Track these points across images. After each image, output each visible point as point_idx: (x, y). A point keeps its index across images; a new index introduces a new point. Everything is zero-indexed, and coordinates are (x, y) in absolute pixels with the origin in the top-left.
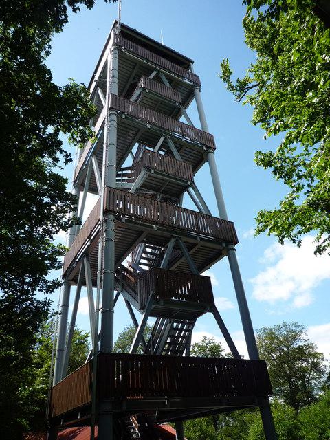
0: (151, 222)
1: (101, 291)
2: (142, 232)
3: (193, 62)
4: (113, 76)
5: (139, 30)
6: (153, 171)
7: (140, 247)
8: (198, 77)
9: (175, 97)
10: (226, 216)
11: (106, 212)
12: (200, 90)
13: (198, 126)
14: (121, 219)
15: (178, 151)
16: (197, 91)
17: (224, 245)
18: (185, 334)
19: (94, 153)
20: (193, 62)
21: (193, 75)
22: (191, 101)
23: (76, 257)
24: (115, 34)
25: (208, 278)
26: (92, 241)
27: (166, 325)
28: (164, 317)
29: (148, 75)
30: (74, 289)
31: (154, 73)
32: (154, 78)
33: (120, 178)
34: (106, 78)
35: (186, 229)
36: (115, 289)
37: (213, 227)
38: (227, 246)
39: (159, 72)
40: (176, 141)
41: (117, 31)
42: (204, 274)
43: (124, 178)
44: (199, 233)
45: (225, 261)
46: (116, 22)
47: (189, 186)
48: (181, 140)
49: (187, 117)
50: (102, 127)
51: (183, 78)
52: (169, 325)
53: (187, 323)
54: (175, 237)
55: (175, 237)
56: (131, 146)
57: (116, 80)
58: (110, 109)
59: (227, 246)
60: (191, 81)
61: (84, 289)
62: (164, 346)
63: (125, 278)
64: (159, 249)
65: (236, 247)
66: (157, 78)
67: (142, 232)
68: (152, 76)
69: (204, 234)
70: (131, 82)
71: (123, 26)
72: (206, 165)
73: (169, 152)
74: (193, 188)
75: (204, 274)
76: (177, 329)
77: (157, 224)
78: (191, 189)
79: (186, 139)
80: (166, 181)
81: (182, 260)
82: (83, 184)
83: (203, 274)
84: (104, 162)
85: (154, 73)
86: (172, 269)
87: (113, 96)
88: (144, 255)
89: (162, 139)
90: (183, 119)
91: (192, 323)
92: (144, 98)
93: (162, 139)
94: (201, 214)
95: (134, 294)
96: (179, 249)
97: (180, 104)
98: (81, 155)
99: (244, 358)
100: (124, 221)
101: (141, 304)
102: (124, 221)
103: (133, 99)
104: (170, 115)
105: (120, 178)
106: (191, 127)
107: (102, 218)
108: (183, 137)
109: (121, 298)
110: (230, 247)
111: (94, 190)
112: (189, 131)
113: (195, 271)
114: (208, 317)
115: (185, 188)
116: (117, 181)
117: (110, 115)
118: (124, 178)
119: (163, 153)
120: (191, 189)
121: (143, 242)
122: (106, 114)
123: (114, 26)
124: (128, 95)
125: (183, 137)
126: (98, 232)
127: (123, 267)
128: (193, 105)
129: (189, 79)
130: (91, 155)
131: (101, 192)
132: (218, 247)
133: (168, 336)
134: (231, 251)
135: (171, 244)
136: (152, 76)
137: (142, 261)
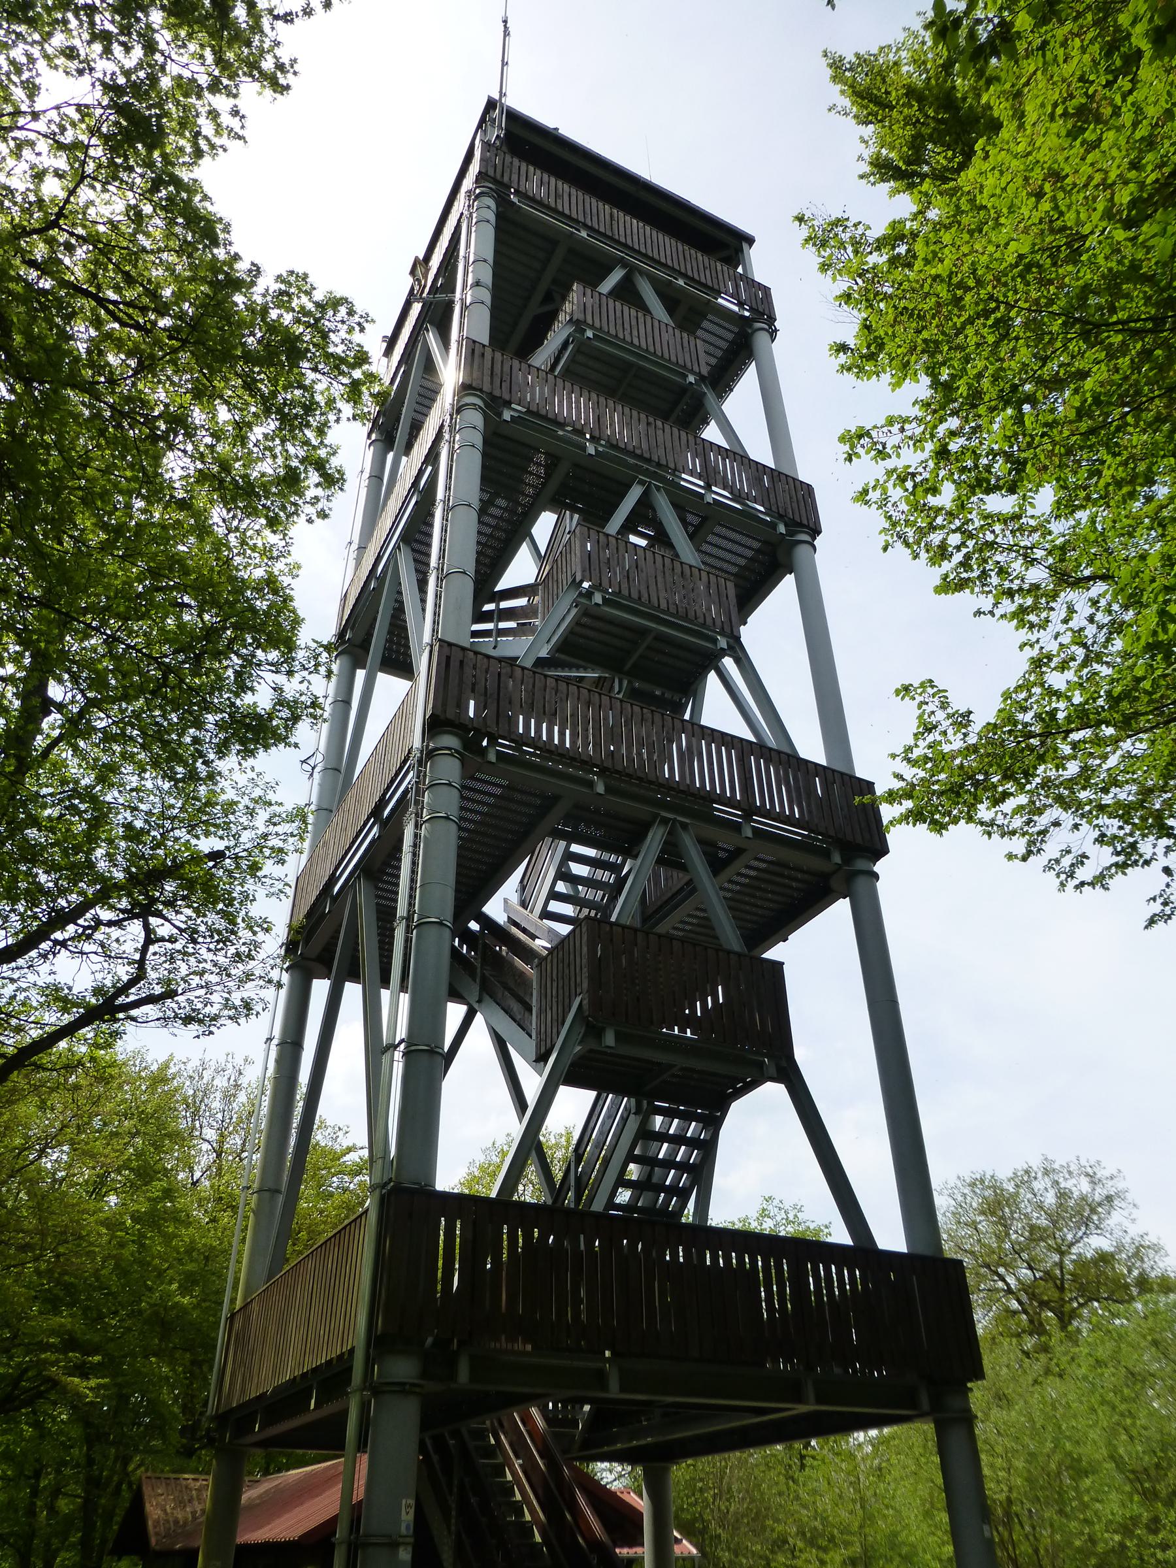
0: (586, 764)
1: (405, 999)
2: (555, 799)
3: (750, 241)
4: (477, 284)
5: (569, 131)
6: (589, 334)
7: (549, 856)
8: (766, 290)
9: (685, 358)
10: (852, 768)
11: (433, 726)
12: (773, 333)
13: (760, 451)
14: (483, 752)
15: (691, 537)
16: (761, 338)
17: (837, 858)
18: (677, 1179)
19: (405, 538)
20: (750, 241)
21: (752, 284)
22: (747, 365)
23: (333, 880)
24: (487, 145)
25: (780, 965)
26: (384, 824)
27: (624, 1120)
28: (620, 1091)
29: (593, 282)
30: (320, 989)
31: (615, 277)
32: (616, 293)
33: (489, 626)
34: (453, 291)
35: (710, 798)
36: (456, 995)
37: (802, 792)
38: (847, 860)
39: (631, 271)
40: (684, 502)
41: (493, 135)
42: (772, 954)
43: (502, 625)
44: (749, 810)
45: (840, 912)
46: (491, 105)
47: (723, 653)
48: (701, 496)
49: (727, 428)
50: (432, 457)
51: (718, 293)
52: (633, 1123)
53: (698, 1118)
54: (665, 821)
55: (665, 821)
56: (530, 517)
57: (486, 296)
58: (465, 388)
59: (847, 860)
60: (740, 304)
61: (353, 993)
62: (613, 1194)
63: (499, 963)
64: (614, 868)
65: (880, 867)
66: (626, 293)
67: (555, 799)
68: (607, 286)
69: (768, 814)
70: (535, 308)
71: (513, 117)
72: (787, 586)
73: (661, 539)
74: (738, 661)
75: (772, 954)
76: (663, 1137)
77: (604, 772)
78: (728, 663)
79: (720, 494)
80: (643, 632)
81: (687, 907)
82: (365, 645)
83: (765, 956)
84: (433, 562)
85: (615, 277)
86: (663, 928)
87: (473, 351)
88: (561, 887)
89: (635, 493)
90: (712, 433)
91: (714, 1123)
92: (580, 358)
93: (635, 493)
94: (759, 749)
95: (516, 1007)
96: (683, 868)
97: (702, 378)
98: (362, 548)
99: (830, 1240)
100: (492, 757)
101: (538, 1047)
102: (492, 757)
103: (542, 357)
104: (665, 417)
105: (489, 626)
106: (737, 455)
107: (417, 742)
108: (708, 487)
109: (479, 1038)
110: (861, 864)
111: (401, 665)
112: (728, 468)
113: (730, 937)
114: (773, 1093)
115: (711, 661)
116: (475, 634)
117: (459, 411)
118: (502, 625)
119: (643, 543)
120: (728, 663)
121: (558, 835)
122: (448, 407)
123: (483, 120)
124: (526, 349)
125: (708, 487)
126: (406, 792)
127: (486, 921)
128: (748, 382)
129: (736, 295)
130: (397, 547)
131: (422, 664)
132: (816, 863)
133: (631, 1158)
134: (861, 883)
135: (654, 840)
136: (607, 286)
137: (555, 907)
